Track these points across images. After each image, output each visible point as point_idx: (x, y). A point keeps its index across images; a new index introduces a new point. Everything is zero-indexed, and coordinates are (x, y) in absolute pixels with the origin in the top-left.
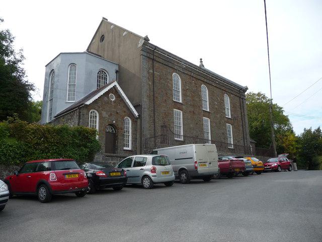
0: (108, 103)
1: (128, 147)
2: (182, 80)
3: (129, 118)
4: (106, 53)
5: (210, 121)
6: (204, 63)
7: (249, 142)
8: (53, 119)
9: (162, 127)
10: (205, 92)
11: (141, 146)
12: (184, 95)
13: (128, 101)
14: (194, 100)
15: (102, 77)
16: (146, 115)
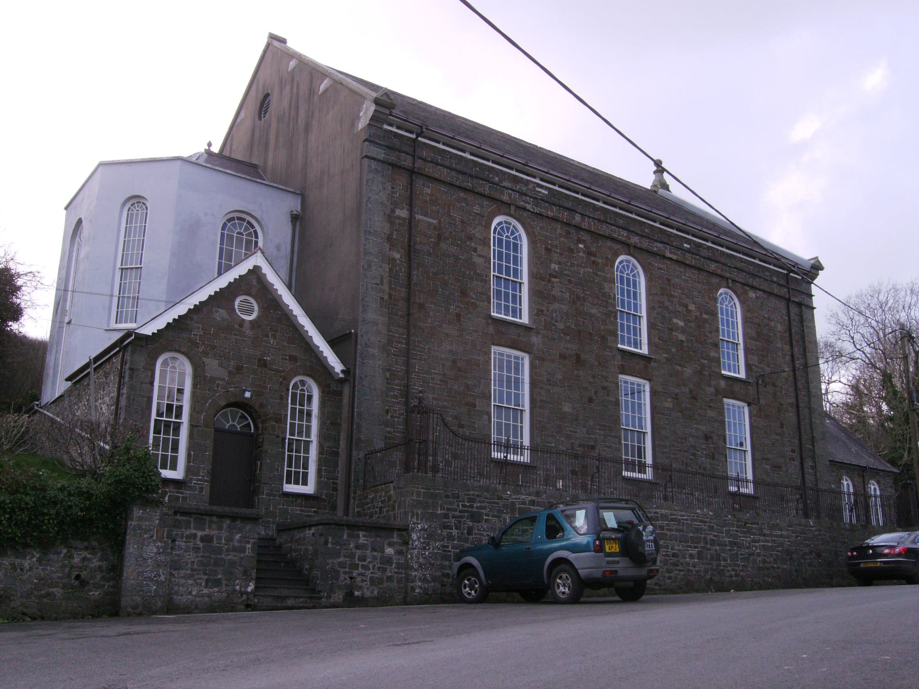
1: (305, 483)
4: (271, 155)
5: (653, 393)
10: (633, 285)
15: (240, 241)
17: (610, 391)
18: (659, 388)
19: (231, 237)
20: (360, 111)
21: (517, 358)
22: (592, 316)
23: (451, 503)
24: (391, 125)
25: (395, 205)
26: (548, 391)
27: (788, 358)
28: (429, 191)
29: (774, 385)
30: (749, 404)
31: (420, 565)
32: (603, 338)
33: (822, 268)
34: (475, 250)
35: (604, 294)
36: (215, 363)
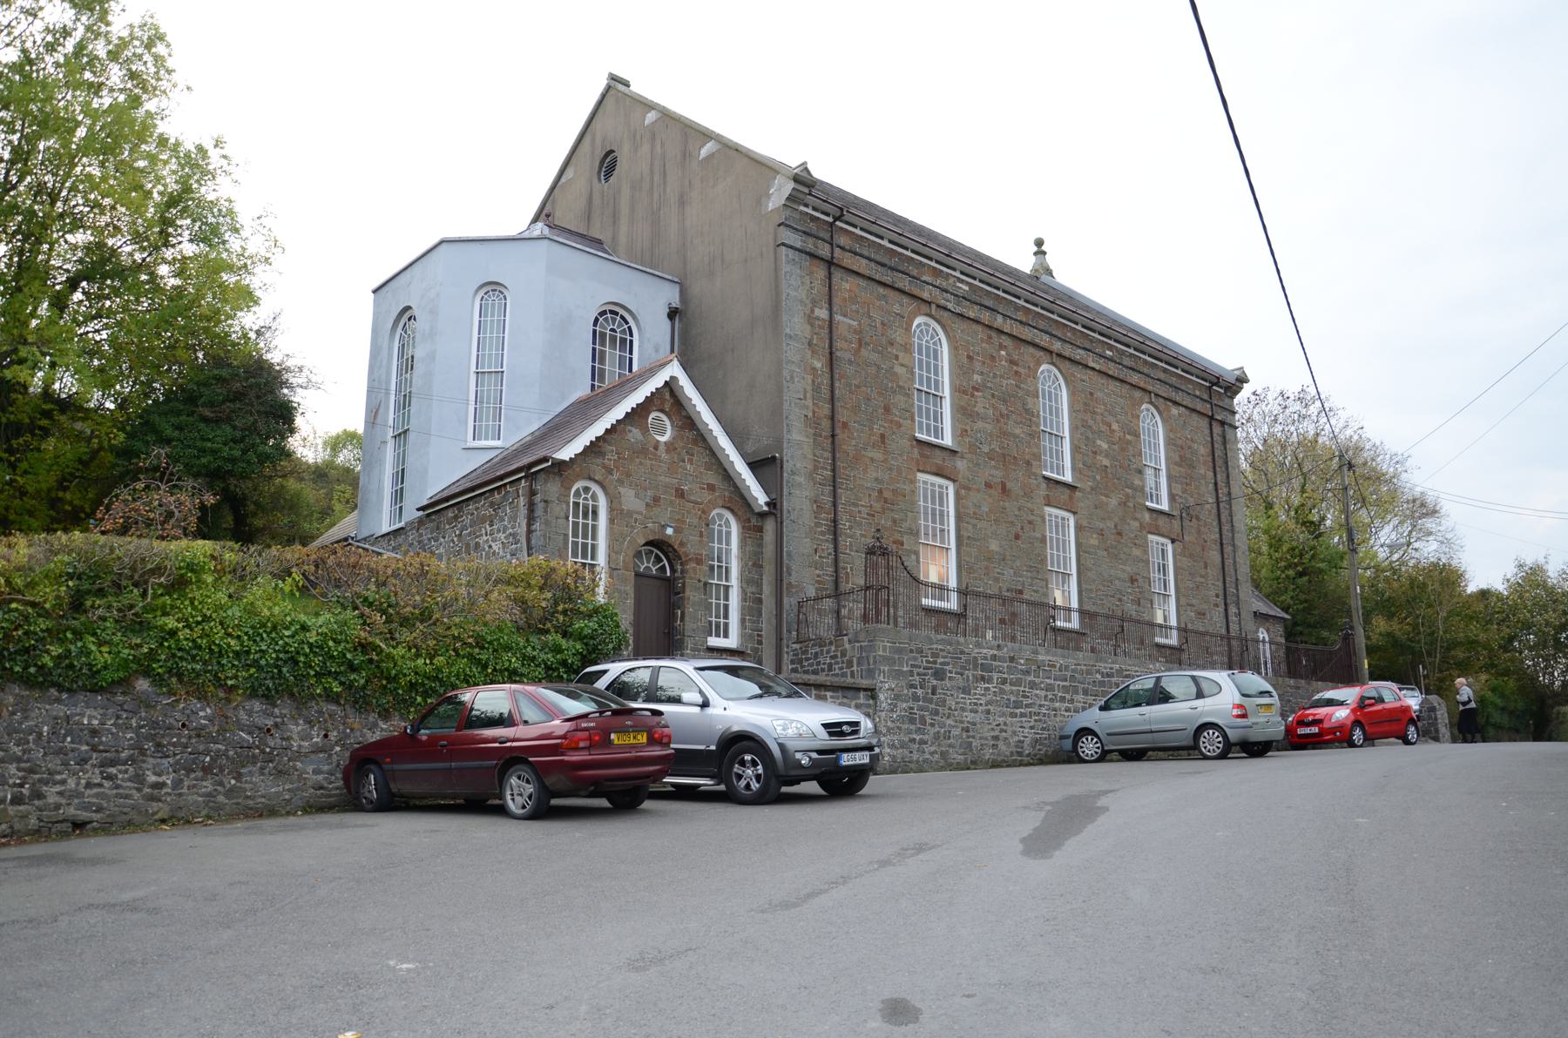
0: (643, 451)
1: (726, 636)
2: (954, 348)
3: (728, 515)
4: (623, 228)
6: (1051, 260)
7: (1247, 616)
8: (410, 514)
9: (870, 552)
11: (779, 639)
12: (963, 412)
13: (724, 442)
14: (1005, 434)
15: (613, 339)
16: (801, 499)
17: (1035, 522)
18: (1085, 523)
19: (603, 335)
20: (769, 188)
21: (941, 487)
22: (1016, 436)
23: (915, 659)
24: (806, 205)
25: (814, 303)
26: (975, 526)
27: (1211, 486)
28: (847, 286)
29: (1198, 518)
30: (1173, 541)
31: (889, 730)
32: (1028, 463)
33: (1247, 381)
34: (897, 357)
35: (1027, 411)
36: (632, 493)
